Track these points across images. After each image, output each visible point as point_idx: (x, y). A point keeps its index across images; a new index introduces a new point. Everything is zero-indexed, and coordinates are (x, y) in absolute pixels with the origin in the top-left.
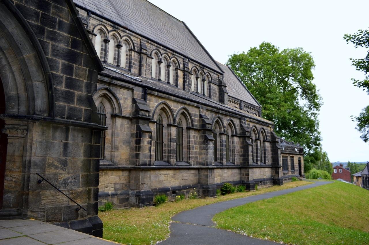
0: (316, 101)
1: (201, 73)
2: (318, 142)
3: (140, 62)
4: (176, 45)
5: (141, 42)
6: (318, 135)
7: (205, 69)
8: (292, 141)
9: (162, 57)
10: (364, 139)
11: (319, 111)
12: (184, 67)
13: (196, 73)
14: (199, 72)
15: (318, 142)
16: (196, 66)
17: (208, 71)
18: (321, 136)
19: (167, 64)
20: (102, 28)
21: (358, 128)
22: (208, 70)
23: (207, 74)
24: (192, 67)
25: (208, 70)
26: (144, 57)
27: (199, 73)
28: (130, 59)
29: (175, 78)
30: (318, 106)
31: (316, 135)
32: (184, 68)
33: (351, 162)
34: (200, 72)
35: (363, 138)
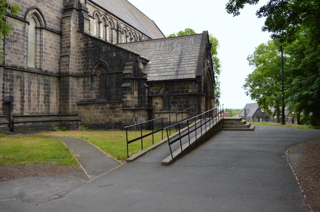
0: (219, 69)
1: (103, 18)
2: (219, 95)
3: (118, 37)
4: (120, 14)
5: (117, 22)
6: (219, 91)
7: (108, 15)
8: (43, 54)
9: (101, 18)
10: (247, 94)
11: (219, 75)
12: (118, 27)
13: (105, 20)
14: (108, 20)
15: (219, 95)
16: (127, 27)
17: (134, 32)
18: (221, 91)
19: (104, 24)
20: (97, 13)
21: (243, 87)
22: (130, 28)
23: (134, 34)
24: (94, 11)
25: (130, 28)
26: (119, 33)
27: (128, 33)
28: (112, 35)
29: (111, 36)
30: (219, 71)
31: (217, 91)
32: (118, 29)
33: (228, 108)
34: (109, 20)
35: (246, 93)
